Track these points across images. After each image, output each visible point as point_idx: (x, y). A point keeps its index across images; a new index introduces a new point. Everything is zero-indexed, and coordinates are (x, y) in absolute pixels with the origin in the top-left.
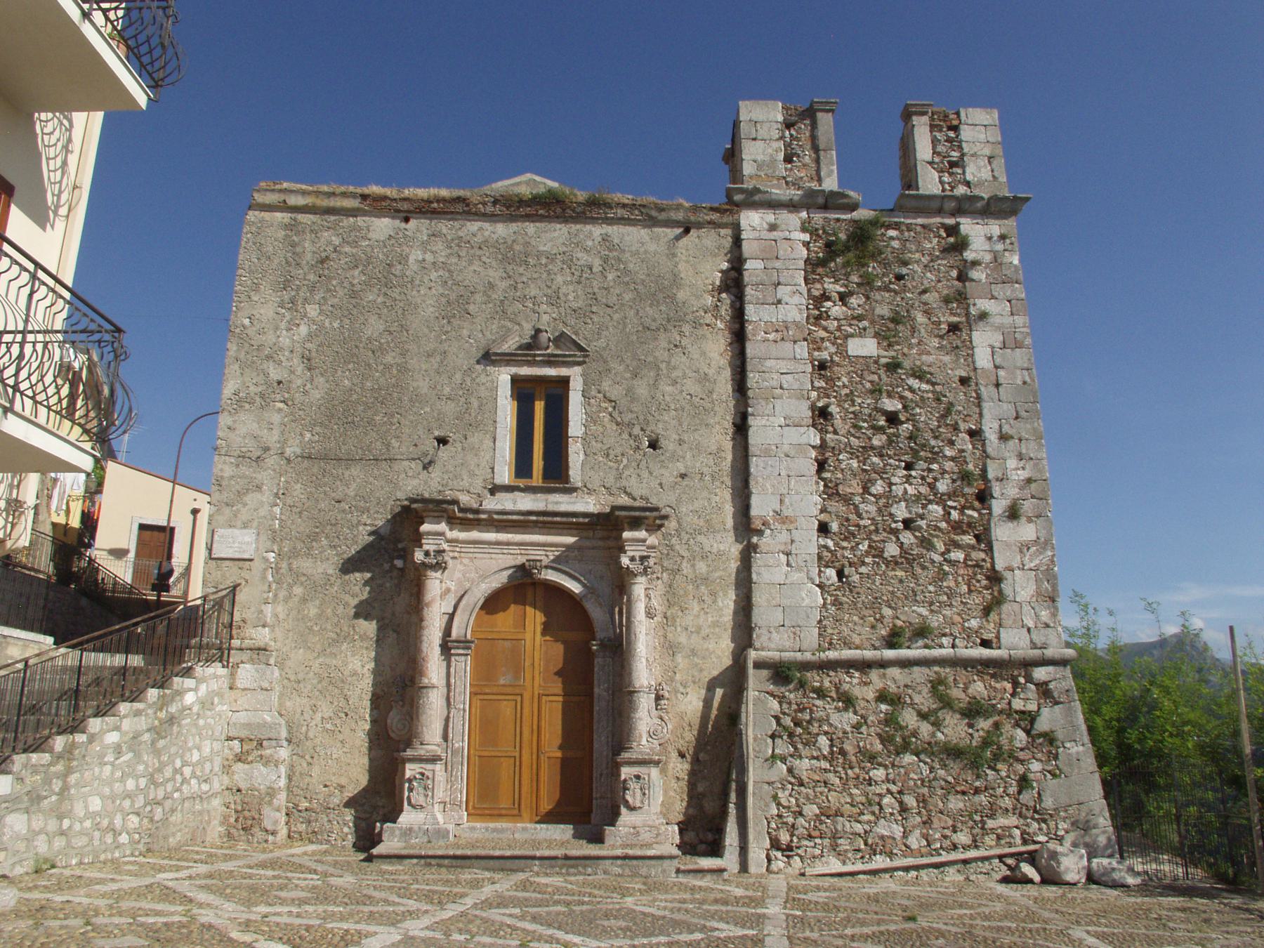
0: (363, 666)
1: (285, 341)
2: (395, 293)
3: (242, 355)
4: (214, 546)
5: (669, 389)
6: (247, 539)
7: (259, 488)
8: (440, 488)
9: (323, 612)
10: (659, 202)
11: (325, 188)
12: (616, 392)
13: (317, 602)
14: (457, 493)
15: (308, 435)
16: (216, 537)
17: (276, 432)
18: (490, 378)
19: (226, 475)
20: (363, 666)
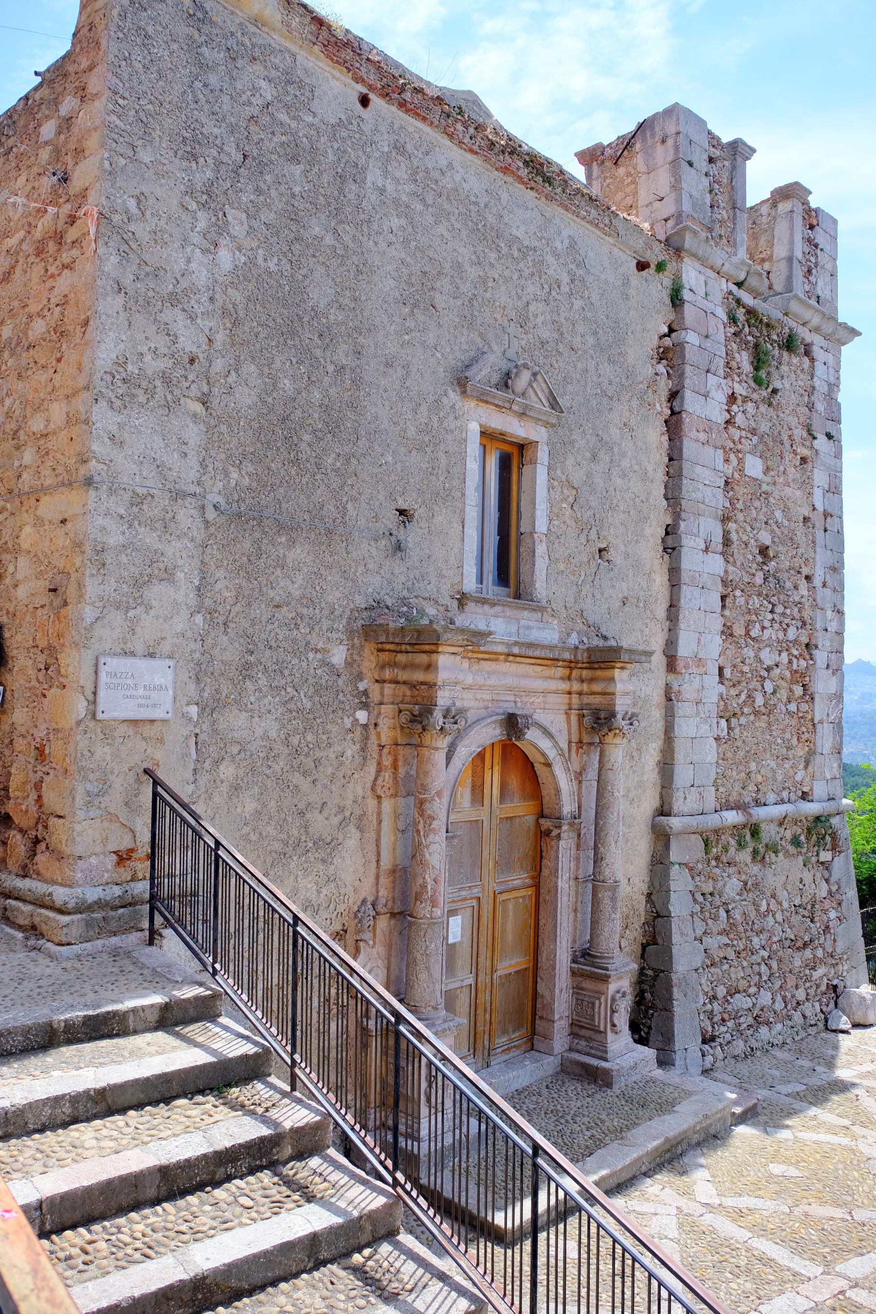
0: (319, 892)
1: (201, 277)
2: (348, 232)
3: (127, 281)
4: (102, 693)
5: (619, 481)
6: (158, 680)
7: (169, 575)
8: (405, 593)
9: (264, 805)
10: (604, 1172)
11: (424, 1085)
12: (577, 477)
13: (256, 790)
14: (424, 603)
15: (235, 475)
16: (103, 678)
17: (193, 461)
18: (459, 423)
19: (112, 541)
20: (319, 892)
